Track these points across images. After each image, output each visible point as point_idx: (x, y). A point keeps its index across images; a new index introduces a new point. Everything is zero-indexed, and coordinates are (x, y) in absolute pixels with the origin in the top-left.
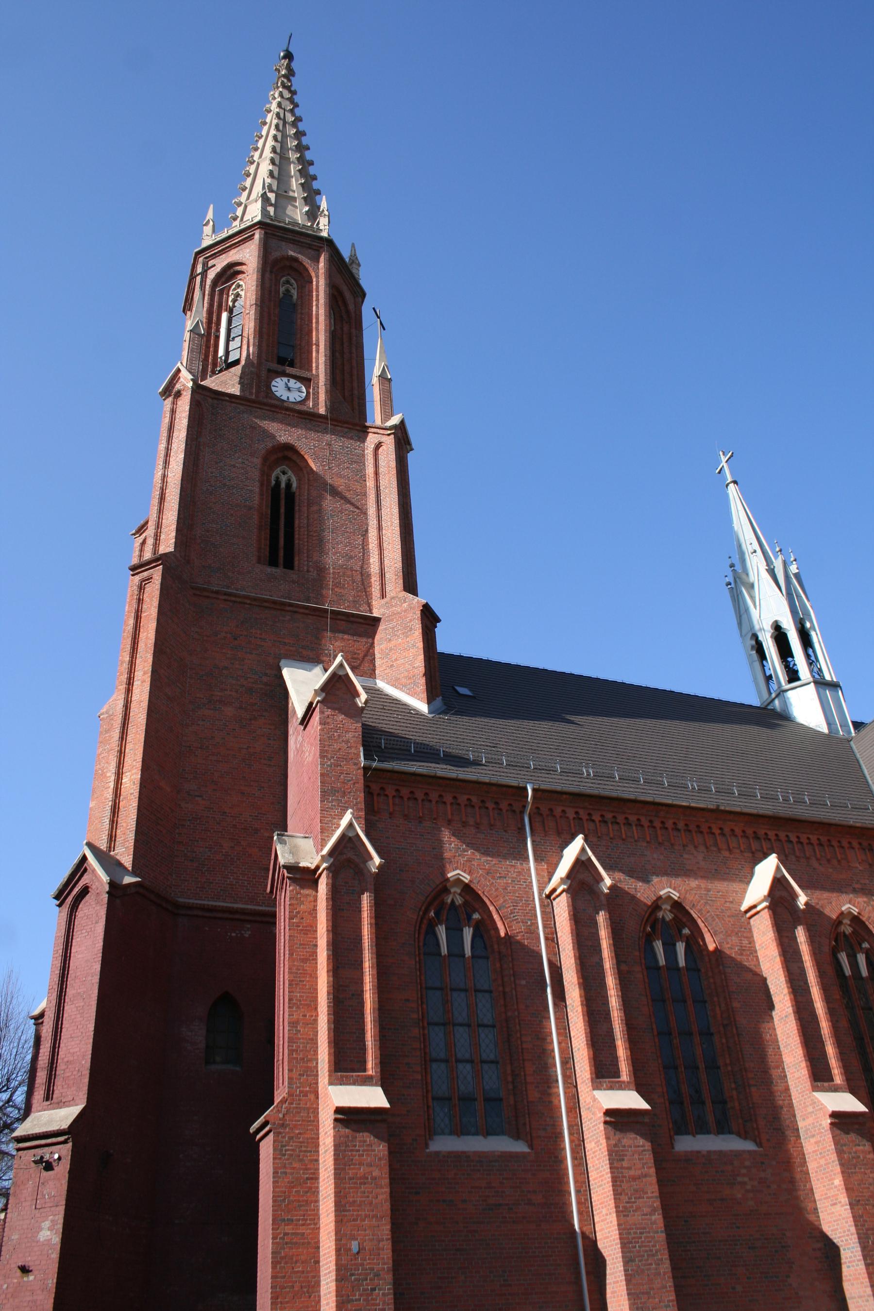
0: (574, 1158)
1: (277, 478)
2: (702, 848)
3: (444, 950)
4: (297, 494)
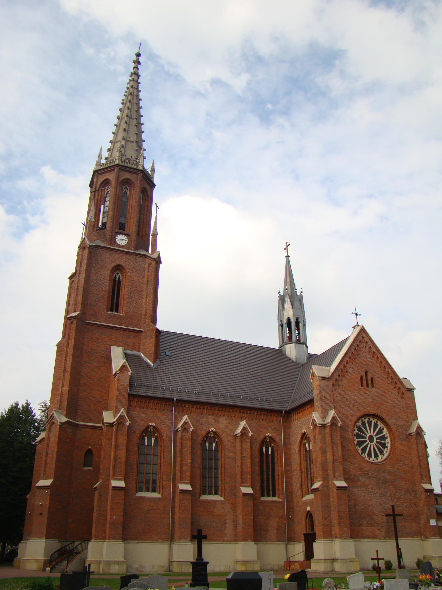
1: (116, 276)
2: (226, 416)
3: (146, 444)
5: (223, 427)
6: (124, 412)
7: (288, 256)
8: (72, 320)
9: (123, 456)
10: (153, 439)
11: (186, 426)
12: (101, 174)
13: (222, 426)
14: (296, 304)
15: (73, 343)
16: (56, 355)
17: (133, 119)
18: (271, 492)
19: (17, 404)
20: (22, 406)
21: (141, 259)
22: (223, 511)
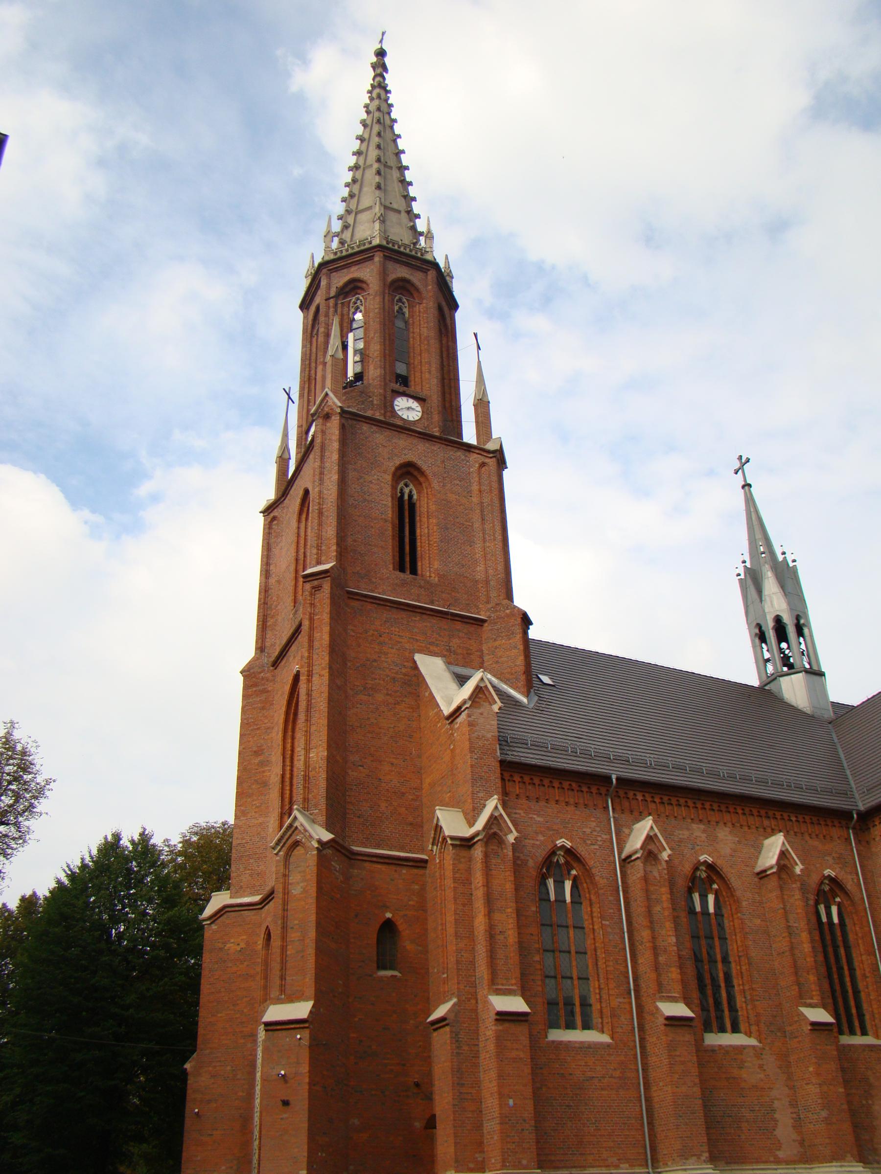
0: (640, 1047)
1: (401, 489)
2: (729, 824)
4: (418, 505)
5: (728, 851)
6: (500, 807)
7: (747, 486)
8: (316, 583)
9: (511, 926)
10: (568, 885)
11: (651, 847)
12: (336, 270)
13: (726, 850)
14: (789, 584)
15: (326, 638)
16: (244, 696)
17: (391, 168)
18: (856, 1024)
19: (117, 837)
20: (132, 842)
21: (459, 453)
22: (762, 1076)
